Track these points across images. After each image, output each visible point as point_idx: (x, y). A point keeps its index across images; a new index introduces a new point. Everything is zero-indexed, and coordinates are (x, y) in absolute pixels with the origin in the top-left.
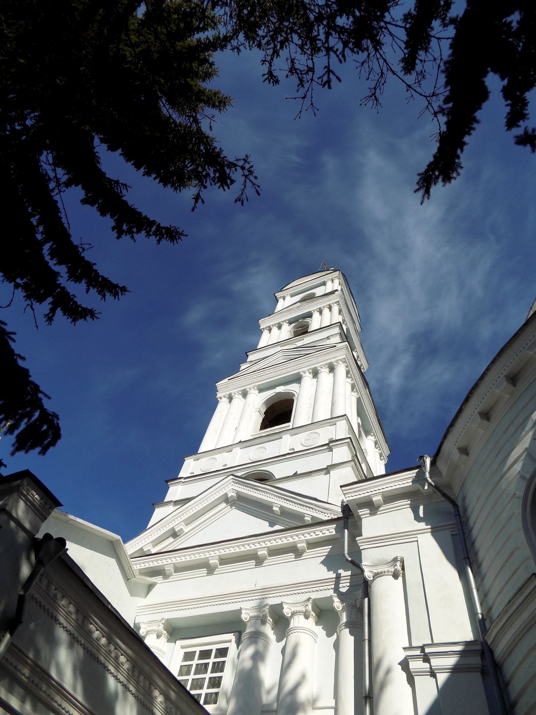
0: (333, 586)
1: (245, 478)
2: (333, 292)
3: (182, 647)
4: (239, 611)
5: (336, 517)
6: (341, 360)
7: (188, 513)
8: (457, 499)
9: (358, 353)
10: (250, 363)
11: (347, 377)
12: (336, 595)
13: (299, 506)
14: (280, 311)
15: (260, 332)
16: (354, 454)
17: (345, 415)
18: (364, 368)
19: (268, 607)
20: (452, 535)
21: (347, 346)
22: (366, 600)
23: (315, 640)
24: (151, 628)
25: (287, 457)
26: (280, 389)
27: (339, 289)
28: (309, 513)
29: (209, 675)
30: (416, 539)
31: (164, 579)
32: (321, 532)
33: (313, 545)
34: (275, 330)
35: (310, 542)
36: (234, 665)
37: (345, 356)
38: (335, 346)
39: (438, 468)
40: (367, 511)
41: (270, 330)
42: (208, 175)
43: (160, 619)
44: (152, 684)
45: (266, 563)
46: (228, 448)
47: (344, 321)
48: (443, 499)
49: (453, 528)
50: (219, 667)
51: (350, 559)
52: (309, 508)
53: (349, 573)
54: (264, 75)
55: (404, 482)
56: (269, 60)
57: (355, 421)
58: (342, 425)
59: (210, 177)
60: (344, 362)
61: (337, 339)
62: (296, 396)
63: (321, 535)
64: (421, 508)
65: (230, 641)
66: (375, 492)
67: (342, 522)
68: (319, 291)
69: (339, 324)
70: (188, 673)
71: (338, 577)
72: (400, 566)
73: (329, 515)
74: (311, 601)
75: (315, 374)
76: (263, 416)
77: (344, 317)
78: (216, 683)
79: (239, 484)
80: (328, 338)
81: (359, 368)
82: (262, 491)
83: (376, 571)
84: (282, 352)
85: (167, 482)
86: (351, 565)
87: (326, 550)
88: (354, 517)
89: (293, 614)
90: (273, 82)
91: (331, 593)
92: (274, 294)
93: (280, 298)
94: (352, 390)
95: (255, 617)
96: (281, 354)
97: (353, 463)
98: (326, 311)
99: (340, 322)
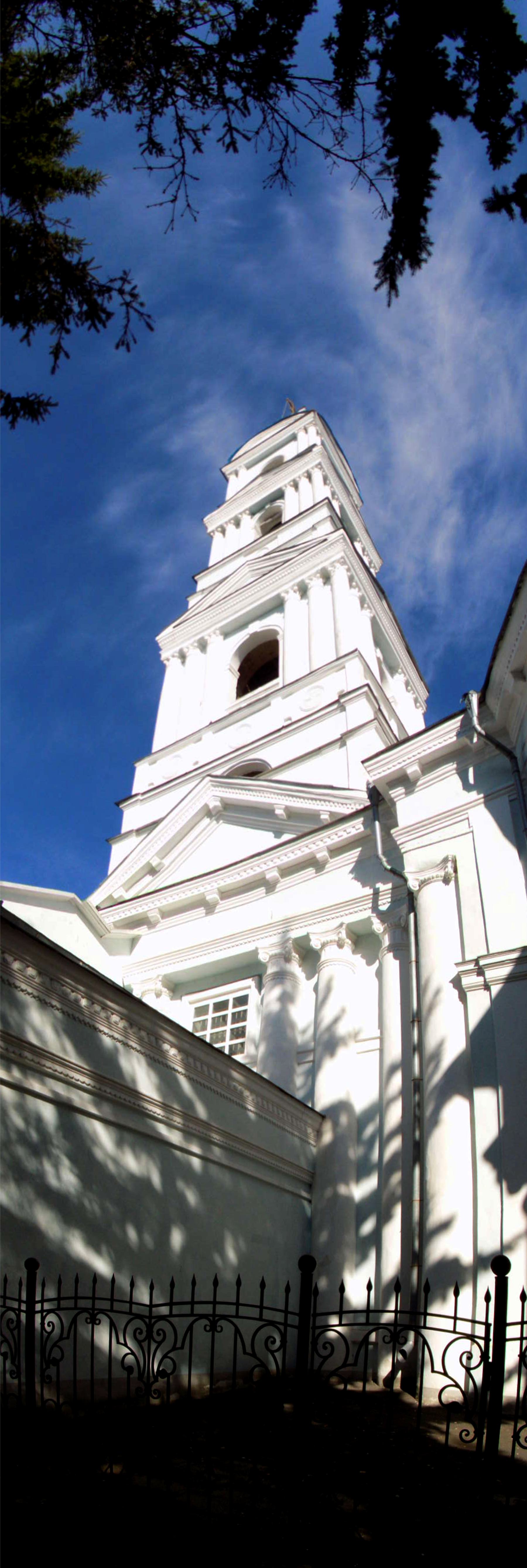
0: (370, 905)
1: (228, 777)
2: (309, 450)
3: (191, 1003)
4: (255, 952)
5: (362, 807)
6: (338, 561)
7: (159, 842)
8: (515, 748)
9: (363, 543)
10: (202, 593)
11: (351, 586)
12: (375, 915)
13: (310, 801)
14: (232, 498)
15: (208, 540)
16: (376, 708)
17: (356, 650)
18: (375, 567)
19: (291, 942)
20: (511, 801)
21: (344, 536)
22: (412, 915)
23: (353, 971)
24: (146, 988)
25: (283, 731)
26: (256, 627)
27: (319, 443)
28: (325, 809)
29: (229, 1027)
30: (466, 816)
31: (149, 928)
32: (345, 831)
33: (336, 851)
34: (230, 528)
35: (332, 848)
36: (259, 1011)
37: (342, 554)
38: (325, 540)
39: (488, 708)
40: (401, 790)
41: (223, 532)
42: (70, 311)
43: (155, 976)
44: (159, 1039)
45: (279, 887)
46: (195, 736)
47: (333, 494)
48: (497, 752)
49: (511, 790)
50: (240, 1017)
51: (389, 867)
52: (325, 801)
53: (390, 886)
54: (141, 145)
55: (445, 738)
56: (147, 123)
57: (372, 655)
58: (354, 666)
59: (74, 313)
60: (344, 563)
61: (328, 527)
62: (281, 633)
63: (345, 836)
64: (471, 771)
65: (249, 987)
66: (408, 761)
67: (370, 813)
68: (288, 452)
69: (327, 501)
70: (204, 1028)
71: (376, 893)
72: (452, 867)
73: (353, 806)
74: (344, 927)
75: (303, 591)
76: (238, 674)
77: (332, 487)
78: (239, 1033)
79: (222, 787)
80: (314, 528)
81: (367, 569)
82: (256, 791)
83: (422, 878)
84: (248, 565)
85: (118, 804)
86: (391, 875)
87: (354, 855)
88: (386, 802)
89: (324, 945)
90: (156, 152)
91: (369, 913)
92: (220, 470)
93: (231, 474)
94: (362, 607)
95: (276, 955)
96: (246, 569)
97: (376, 723)
98: (304, 483)
99: (327, 498)
